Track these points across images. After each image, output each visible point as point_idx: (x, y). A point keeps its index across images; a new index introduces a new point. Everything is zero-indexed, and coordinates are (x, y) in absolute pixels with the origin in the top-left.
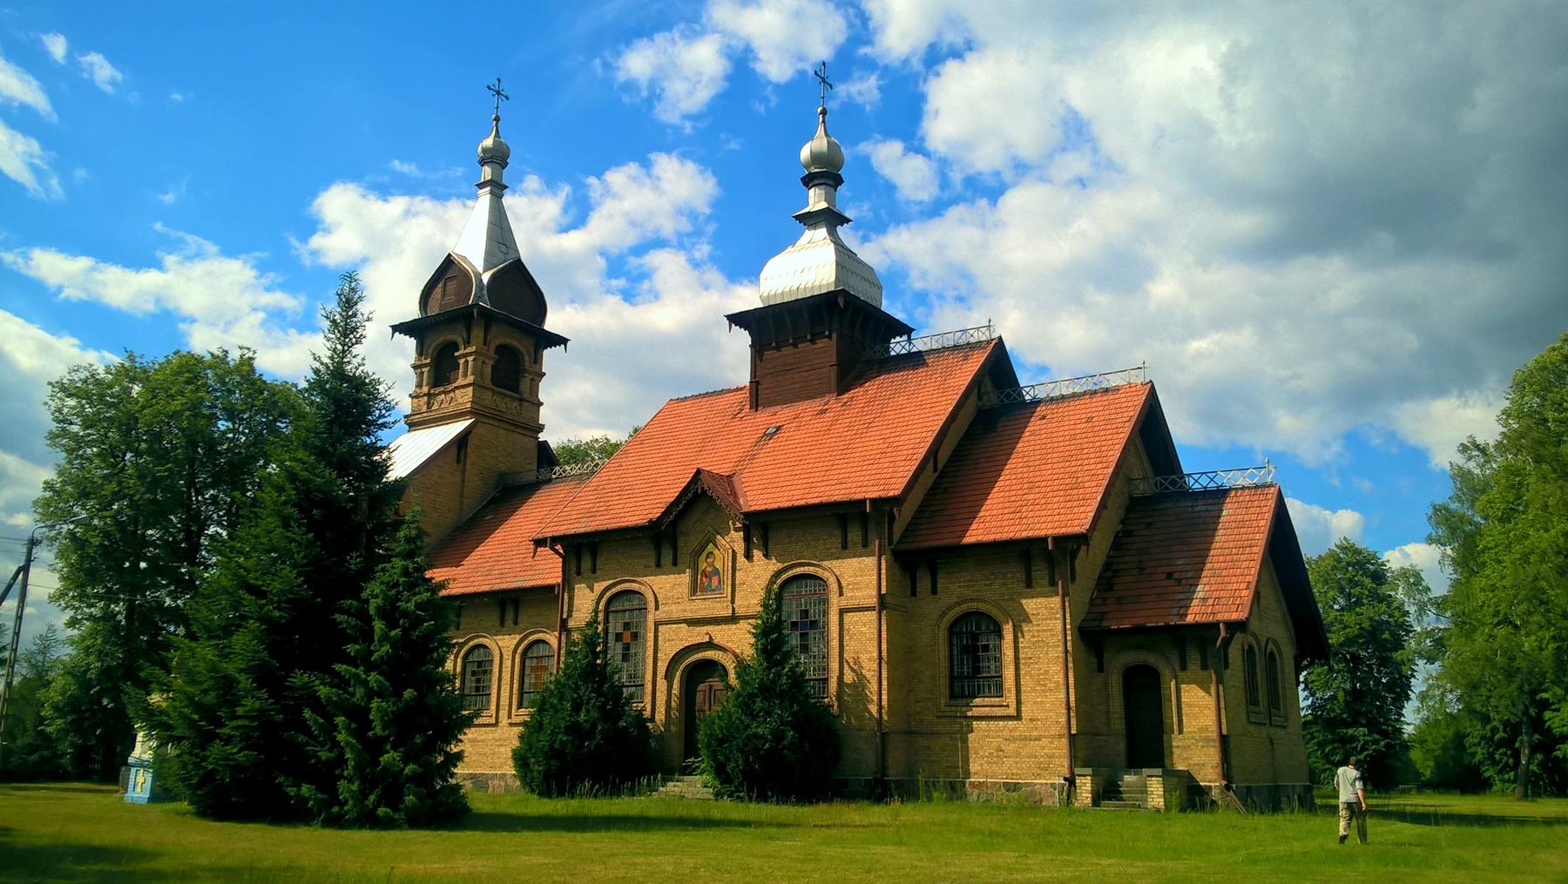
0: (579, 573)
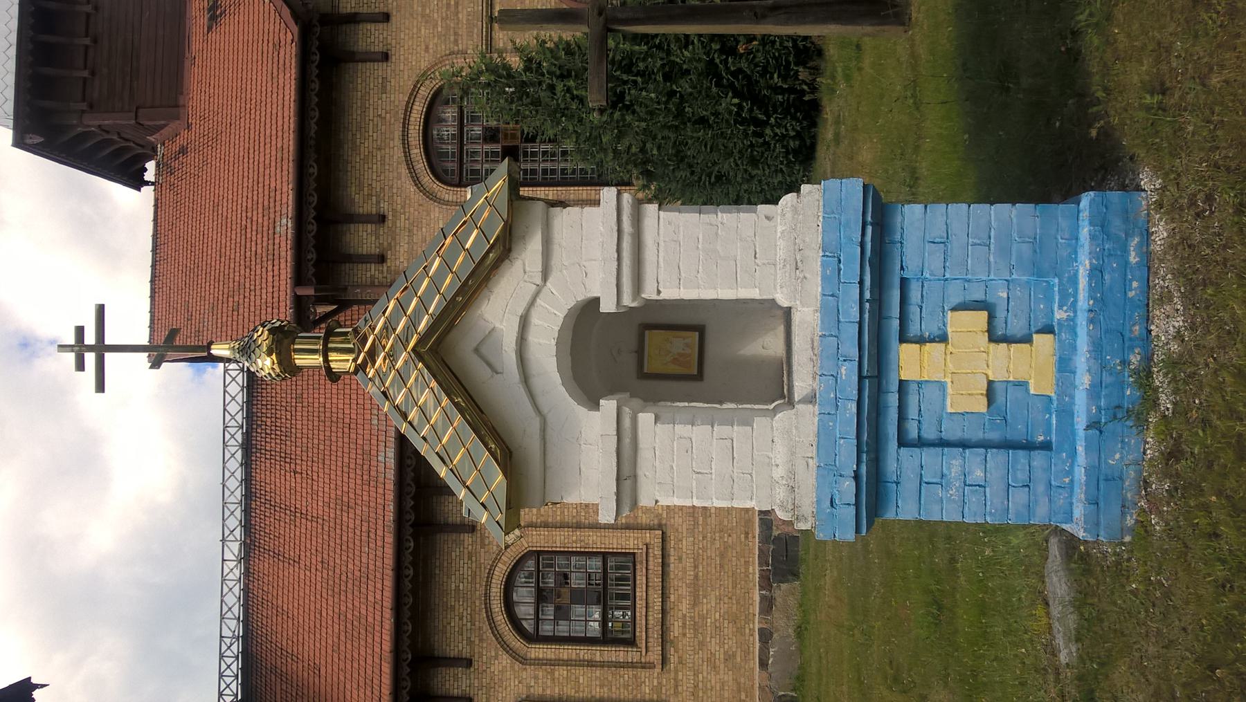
0: (382, 259)
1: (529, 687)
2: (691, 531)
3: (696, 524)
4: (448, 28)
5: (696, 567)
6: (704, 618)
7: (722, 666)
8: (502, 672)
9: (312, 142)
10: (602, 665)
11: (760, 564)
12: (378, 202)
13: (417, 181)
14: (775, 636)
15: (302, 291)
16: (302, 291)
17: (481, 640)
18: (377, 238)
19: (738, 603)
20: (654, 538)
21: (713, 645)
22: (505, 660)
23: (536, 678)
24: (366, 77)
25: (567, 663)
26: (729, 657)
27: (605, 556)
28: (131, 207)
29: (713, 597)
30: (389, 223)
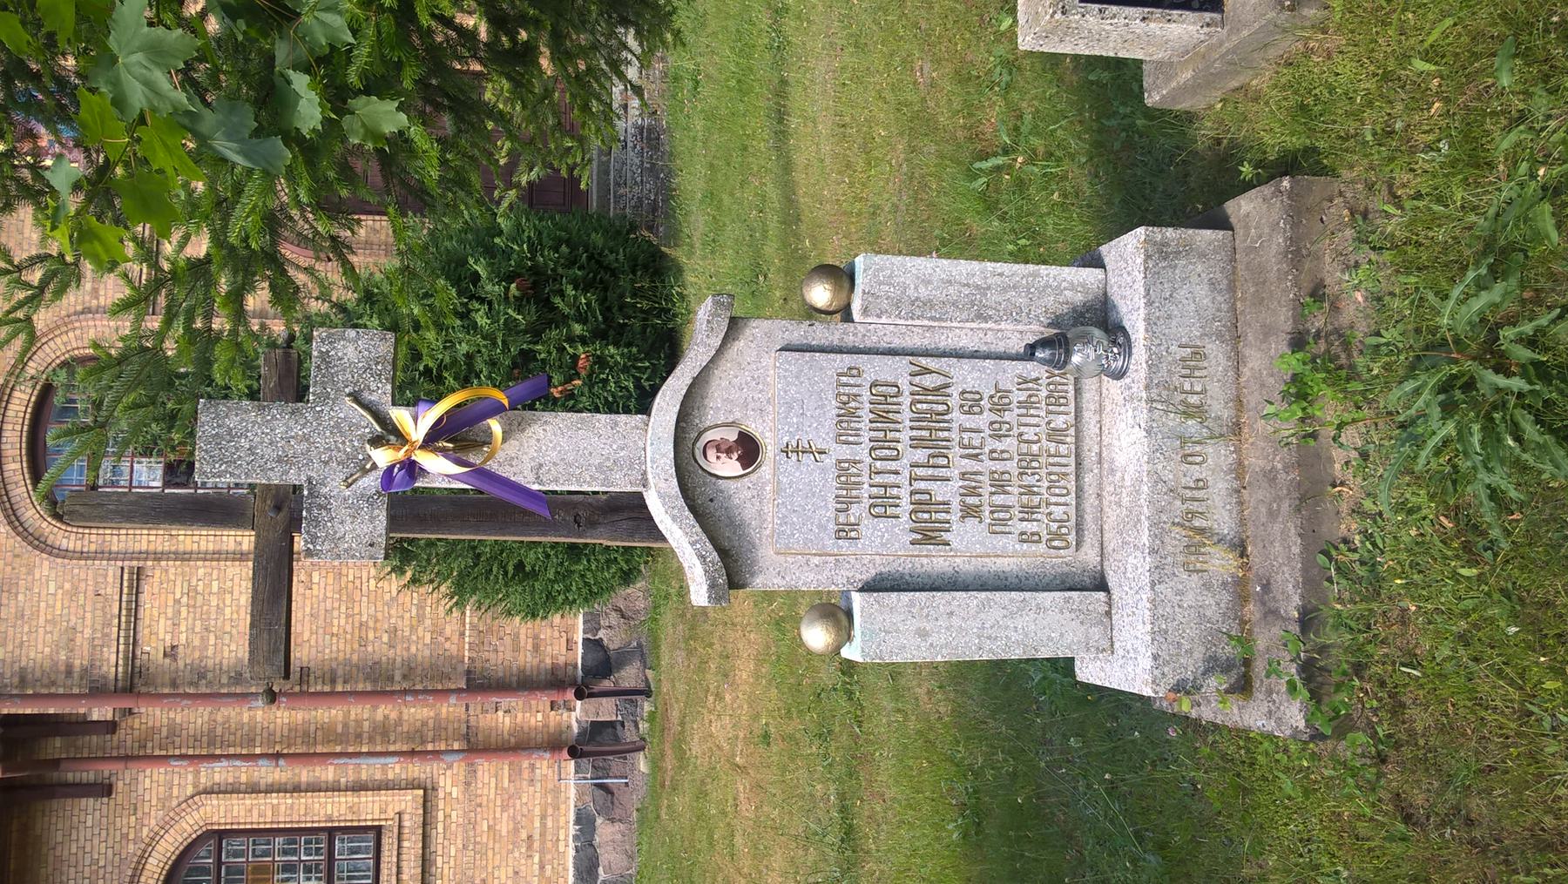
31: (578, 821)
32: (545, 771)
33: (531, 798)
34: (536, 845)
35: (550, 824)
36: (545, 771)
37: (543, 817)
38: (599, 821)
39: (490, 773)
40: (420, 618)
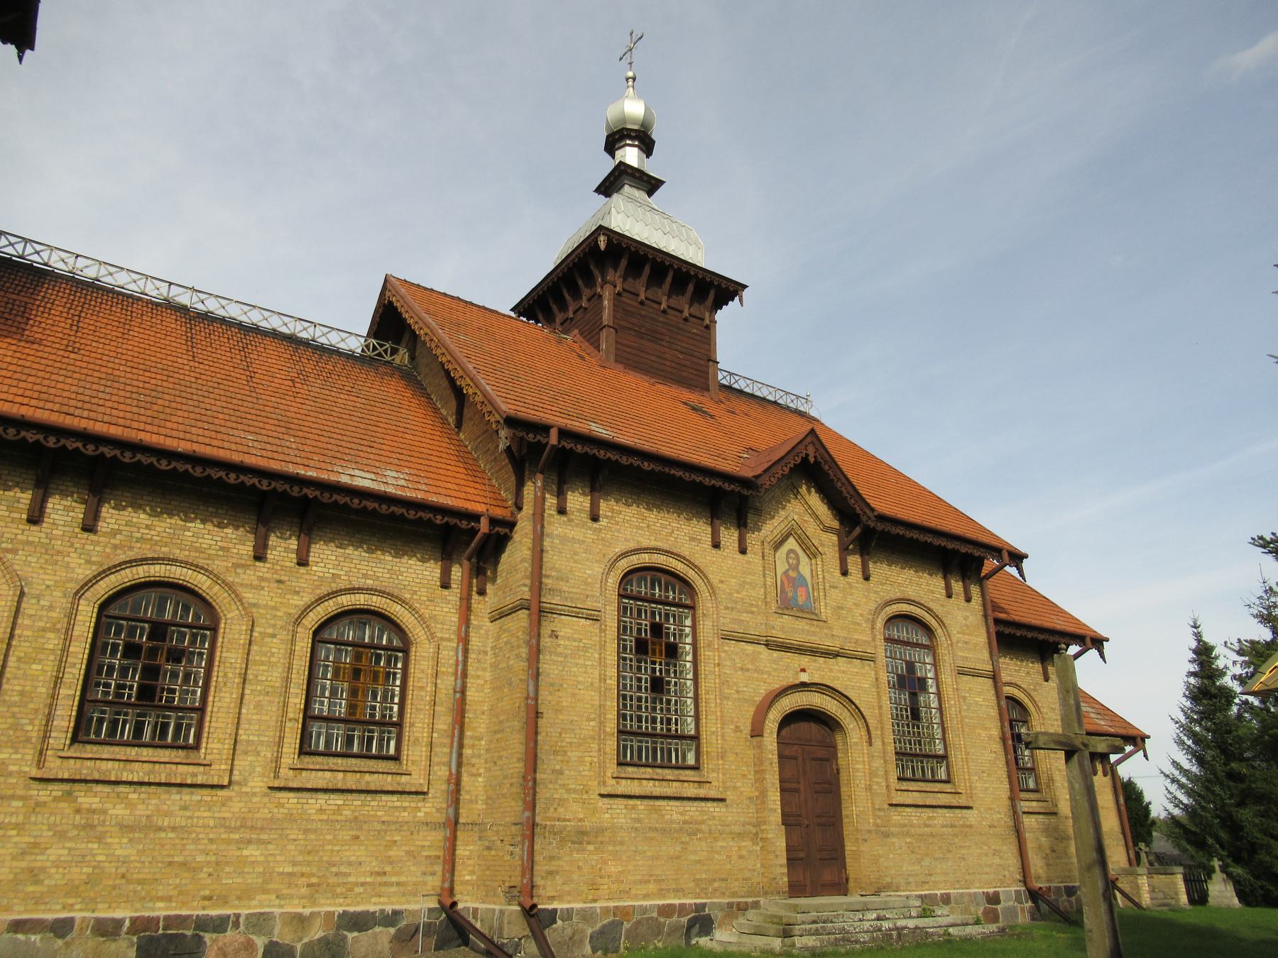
1: (38, 598)
2: (223, 824)
3: (231, 830)
4: (736, 602)
5: (174, 829)
6: (100, 839)
7: (24, 864)
8: (67, 566)
9: (667, 470)
10: (54, 696)
11: (167, 918)
12: (607, 517)
13: (625, 555)
14: (60, 942)
15: (554, 434)
16: (554, 434)
17: (115, 547)
18: (579, 510)
19: (114, 887)
20: (217, 774)
21: (57, 852)
22: (84, 572)
23: (51, 608)
24: (701, 529)
25: (65, 650)
26: (34, 875)
27: (202, 710)
28: (505, 307)
29: (130, 851)
30: (590, 523)
31: (395, 913)
32: (430, 884)
33: (412, 873)
34: (379, 879)
35: (393, 889)
36: (430, 884)
37: (398, 884)
38: (392, 930)
39: (432, 841)
40: (569, 791)
